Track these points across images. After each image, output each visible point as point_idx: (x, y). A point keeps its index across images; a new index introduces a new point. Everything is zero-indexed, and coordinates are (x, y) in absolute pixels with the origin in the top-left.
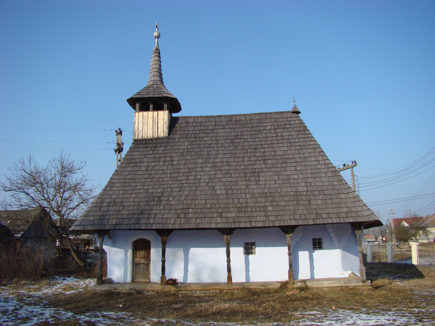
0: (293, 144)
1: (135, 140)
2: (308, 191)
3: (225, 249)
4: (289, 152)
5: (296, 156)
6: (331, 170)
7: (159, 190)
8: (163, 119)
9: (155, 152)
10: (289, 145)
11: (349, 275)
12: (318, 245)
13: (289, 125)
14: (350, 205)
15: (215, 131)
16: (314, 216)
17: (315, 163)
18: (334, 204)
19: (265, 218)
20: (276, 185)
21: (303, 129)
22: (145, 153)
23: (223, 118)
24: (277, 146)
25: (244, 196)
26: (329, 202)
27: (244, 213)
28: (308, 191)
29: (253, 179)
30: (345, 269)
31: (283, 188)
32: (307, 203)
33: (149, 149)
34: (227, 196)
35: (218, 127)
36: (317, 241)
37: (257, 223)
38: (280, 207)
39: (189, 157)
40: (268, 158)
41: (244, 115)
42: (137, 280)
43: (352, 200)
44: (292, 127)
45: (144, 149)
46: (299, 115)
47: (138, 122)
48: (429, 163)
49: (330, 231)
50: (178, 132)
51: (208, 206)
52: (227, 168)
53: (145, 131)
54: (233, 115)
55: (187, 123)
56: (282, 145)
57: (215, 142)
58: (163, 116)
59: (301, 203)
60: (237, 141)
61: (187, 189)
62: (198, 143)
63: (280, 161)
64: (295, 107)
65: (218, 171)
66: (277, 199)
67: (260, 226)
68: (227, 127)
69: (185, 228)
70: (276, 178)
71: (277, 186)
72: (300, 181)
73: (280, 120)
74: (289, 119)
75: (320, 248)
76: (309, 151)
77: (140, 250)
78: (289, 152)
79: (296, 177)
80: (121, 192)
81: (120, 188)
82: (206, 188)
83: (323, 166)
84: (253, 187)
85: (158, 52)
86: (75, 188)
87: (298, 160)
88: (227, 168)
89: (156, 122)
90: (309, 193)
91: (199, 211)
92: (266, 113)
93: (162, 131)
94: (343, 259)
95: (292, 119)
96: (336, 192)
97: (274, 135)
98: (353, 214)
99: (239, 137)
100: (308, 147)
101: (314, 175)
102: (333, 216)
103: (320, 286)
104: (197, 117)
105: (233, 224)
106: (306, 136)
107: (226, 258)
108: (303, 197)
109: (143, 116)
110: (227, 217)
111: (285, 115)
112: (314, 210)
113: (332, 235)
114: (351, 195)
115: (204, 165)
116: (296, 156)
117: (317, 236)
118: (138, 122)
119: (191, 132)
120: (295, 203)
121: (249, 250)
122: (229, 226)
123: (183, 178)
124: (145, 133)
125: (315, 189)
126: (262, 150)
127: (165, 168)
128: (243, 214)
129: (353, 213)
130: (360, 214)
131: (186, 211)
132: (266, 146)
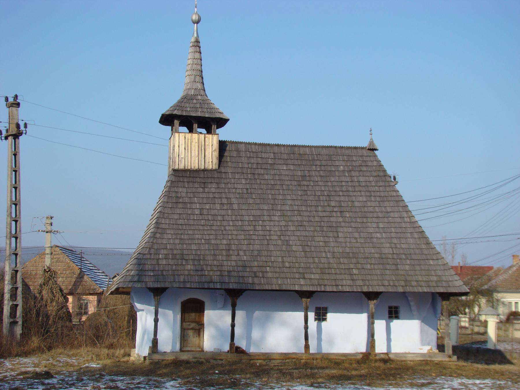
0: (373, 194)
2: (394, 254)
4: (369, 204)
5: (377, 209)
6: (417, 230)
7: (225, 242)
8: (212, 145)
10: (368, 194)
11: (428, 350)
12: (394, 314)
14: (439, 273)
15: (276, 167)
16: (403, 283)
17: (399, 220)
18: (423, 271)
19: (351, 281)
20: (358, 244)
23: (282, 148)
24: (355, 194)
25: (324, 254)
26: (418, 268)
27: (328, 275)
28: (394, 254)
29: (331, 234)
31: (365, 249)
32: (393, 267)
33: (196, 185)
34: (305, 254)
35: (279, 162)
36: (393, 310)
38: (366, 271)
39: (251, 201)
40: (345, 209)
41: (308, 146)
42: (185, 349)
43: (442, 268)
44: (369, 170)
45: (191, 185)
46: (376, 152)
47: (179, 146)
48: (509, 182)
49: (410, 299)
50: (230, 164)
51: (287, 265)
52: (299, 218)
53: (188, 159)
55: (238, 151)
56: (359, 193)
57: (278, 182)
58: (212, 142)
59: (388, 267)
63: (360, 215)
64: (371, 142)
65: (289, 222)
66: (362, 261)
67: (348, 290)
68: (289, 162)
69: (267, 288)
70: (356, 235)
71: (358, 245)
72: (383, 241)
75: (397, 317)
76: (392, 204)
79: (378, 235)
81: (174, 237)
82: (280, 242)
83: (408, 225)
84: (332, 244)
85: (197, 44)
87: (380, 215)
88: (299, 218)
89: (202, 149)
90: (395, 256)
92: (336, 147)
93: (211, 161)
94: (422, 331)
96: (424, 257)
97: (349, 179)
98: (444, 284)
99: (308, 178)
100: (390, 199)
101: (399, 235)
103: (404, 359)
104: (249, 144)
105: (318, 286)
106: (387, 184)
108: (389, 260)
109: (185, 138)
110: (311, 279)
111: (360, 152)
112: (403, 276)
113: (412, 304)
114: (440, 262)
115: (272, 213)
116: (377, 209)
117: (394, 304)
118: (179, 146)
119: (246, 166)
120: (381, 266)
121: (321, 316)
122: (311, 289)
124: (188, 162)
125: (402, 252)
126: (337, 199)
127: (223, 212)
128: (327, 277)
129: (443, 282)
130: (450, 284)
132: (341, 193)
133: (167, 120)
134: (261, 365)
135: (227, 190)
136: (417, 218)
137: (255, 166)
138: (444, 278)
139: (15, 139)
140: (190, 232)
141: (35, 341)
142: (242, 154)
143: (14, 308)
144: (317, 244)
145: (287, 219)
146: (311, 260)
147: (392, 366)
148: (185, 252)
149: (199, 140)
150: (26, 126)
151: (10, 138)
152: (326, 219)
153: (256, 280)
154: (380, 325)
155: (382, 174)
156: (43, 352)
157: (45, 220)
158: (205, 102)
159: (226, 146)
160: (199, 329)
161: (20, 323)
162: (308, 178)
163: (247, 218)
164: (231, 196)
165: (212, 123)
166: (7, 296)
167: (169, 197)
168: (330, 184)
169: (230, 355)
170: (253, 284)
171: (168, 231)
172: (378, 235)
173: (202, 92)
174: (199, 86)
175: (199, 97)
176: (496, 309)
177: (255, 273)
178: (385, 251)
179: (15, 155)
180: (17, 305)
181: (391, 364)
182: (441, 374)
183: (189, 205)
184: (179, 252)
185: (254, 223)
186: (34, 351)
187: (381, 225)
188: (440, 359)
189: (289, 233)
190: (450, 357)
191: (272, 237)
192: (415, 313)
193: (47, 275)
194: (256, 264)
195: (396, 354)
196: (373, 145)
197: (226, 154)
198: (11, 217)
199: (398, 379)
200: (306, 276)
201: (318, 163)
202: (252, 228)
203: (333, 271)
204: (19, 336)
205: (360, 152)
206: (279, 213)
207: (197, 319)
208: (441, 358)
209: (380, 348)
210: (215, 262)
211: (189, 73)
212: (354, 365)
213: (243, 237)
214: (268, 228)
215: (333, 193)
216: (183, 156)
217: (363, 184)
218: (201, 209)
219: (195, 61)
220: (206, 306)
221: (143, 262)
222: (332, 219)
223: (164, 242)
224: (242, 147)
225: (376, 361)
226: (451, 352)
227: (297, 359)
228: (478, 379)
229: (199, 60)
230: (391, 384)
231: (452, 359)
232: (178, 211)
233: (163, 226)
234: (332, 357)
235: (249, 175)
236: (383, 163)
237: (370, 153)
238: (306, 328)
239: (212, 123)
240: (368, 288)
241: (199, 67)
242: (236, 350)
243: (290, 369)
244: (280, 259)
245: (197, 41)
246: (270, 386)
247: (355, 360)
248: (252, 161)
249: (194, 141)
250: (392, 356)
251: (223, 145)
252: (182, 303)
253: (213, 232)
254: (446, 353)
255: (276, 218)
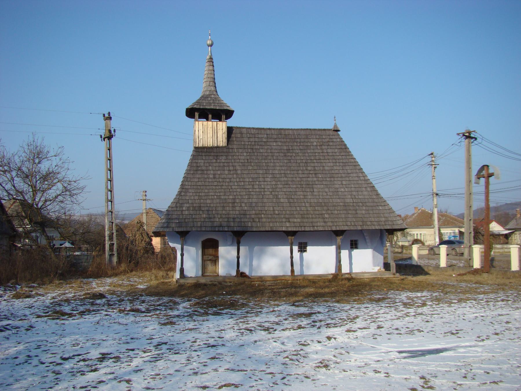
1: (195, 148)
3: (289, 247)
4: (335, 168)
7: (231, 197)
9: (218, 161)
10: (334, 161)
12: (354, 245)
13: (329, 141)
14: (386, 215)
15: (268, 144)
16: (361, 223)
17: (356, 179)
21: (344, 148)
22: (209, 161)
23: (273, 131)
24: (325, 161)
25: (303, 204)
26: (371, 212)
29: (308, 190)
30: (375, 265)
32: (354, 212)
35: (271, 140)
37: (319, 228)
39: (250, 168)
40: (318, 172)
43: (388, 211)
45: (207, 158)
46: (339, 132)
49: (365, 234)
50: (235, 143)
51: (277, 212)
52: (285, 179)
54: (282, 129)
55: (241, 133)
56: (328, 161)
57: (270, 154)
58: (222, 126)
59: (350, 212)
60: (289, 154)
61: (255, 197)
62: (256, 154)
64: (335, 126)
68: (278, 140)
70: (327, 190)
71: (328, 197)
73: (324, 137)
74: (331, 137)
75: (356, 248)
77: (208, 248)
78: (335, 168)
79: (343, 190)
80: (197, 198)
82: (271, 196)
83: (363, 182)
84: (309, 197)
85: (211, 60)
86: (47, 177)
87: (343, 175)
88: (285, 179)
89: (215, 132)
90: (355, 204)
91: (270, 216)
93: (221, 140)
94: (374, 257)
95: (334, 137)
96: (375, 204)
97: (320, 151)
98: (390, 223)
99: (291, 151)
101: (357, 189)
102: (375, 223)
103: (362, 277)
104: (249, 128)
107: (290, 255)
110: (294, 222)
111: (328, 132)
114: (387, 208)
117: (354, 238)
119: (247, 143)
120: (345, 212)
121: (302, 249)
122: (294, 229)
123: (249, 187)
127: (230, 176)
128: (306, 220)
130: (394, 222)
131: (260, 216)
132: (315, 161)
133: (191, 113)
134: (259, 285)
135: (233, 161)
136: (369, 177)
137: (253, 143)
138: (390, 219)
139: (109, 140)
140: (206, 191)
141: (123, 266)
142: (244, 135)
143: (112, 245)
144: (298, 197)
145: (276, 179)
146: (294, 209)
147: (354, 283)
148: (202, 205)
149: (212, 126)
150: (115, 131)
151: (106, 139)
152: (304, 179)
153: (254, 224)
154: (345, 253)
155: (343, 147)
156: (128, 273)
157: (142, 193)
158: (217, 99)
159: (233, 130)
160: (215, 260)
161: (116, 255)
162: (291, 151)
163: (247, 180)
164: (236, 164)
165: (222, 114)
166: (107, 238)
167: (191, 166)
168: (307, 155)
169: (236, 279)
170: (252, 227)
171: (190, 191)
172: (343, 190)
173: (215, 93)
174: (213, 88)
175: (213, 96)
176: (407, 238)
177: (253, 219)
178: (348, 201)
179: (109, 150)
180: (113, 244)
181: (353, 282)
182: (390, 289)
183: (205, 172)
184: (198, 205)
185: (252, 183)
186: (121, 272)
187: (344, 183)
188: (387, 276)
189: (278, 190)
190: (394, 274)
191: (266, 193)
192: (369, 244)
193: (139, 225)
194: (254, 212)
195: (356, 273)
196: (337, 127)
197: (233, 136)
198: (108, 189)
199: (360, 295)
200: (291, 220)
201: (298, 140)
202: (251, 187)
203: (310, 216)
204: (115, 263)
205: (328, 132)
206: (271, 176)
207: (214, 253)
208: (388, 275)
209: (345, 269)
210: (224, 212)
211: (205, 80)
212: (327, 283)
213: (244, 193)
214: (263, 186)
215: (309, 161)
216: (201, 138)
217: (331, 154)
218: (214, 174)
219: (210, 72)
220: (220, 243)
221: (171, 213)
222: (309, 179)
223: (187, 198)
224: (244, 131)
225: (342, 280)
226: (395, 271)
227: (286, 280)
228: (418, 291)
229: (212, 71)
230: (355, 301)
231: (395, 276)
232: (198, 176)
233: (187, 187)
234: (311, 278)
235: (249, 150)
236: (344, 140)
237: (335, 133)
238: (292, 257)
239: (222, 114)
240: (336, 227)
241: (212, 76)
242: (241, 275)
243: (279, 289)
244: (272, 208)
245: (211, 58)
246: (261, 306)
247: (327, 279)
248: (251, 140)
249: (209, 126)
250: (353, 276)
251: (230, 130)
252: (202, 242)
253: (223, 190)
254: (391, 272)
255: (269, 179)
